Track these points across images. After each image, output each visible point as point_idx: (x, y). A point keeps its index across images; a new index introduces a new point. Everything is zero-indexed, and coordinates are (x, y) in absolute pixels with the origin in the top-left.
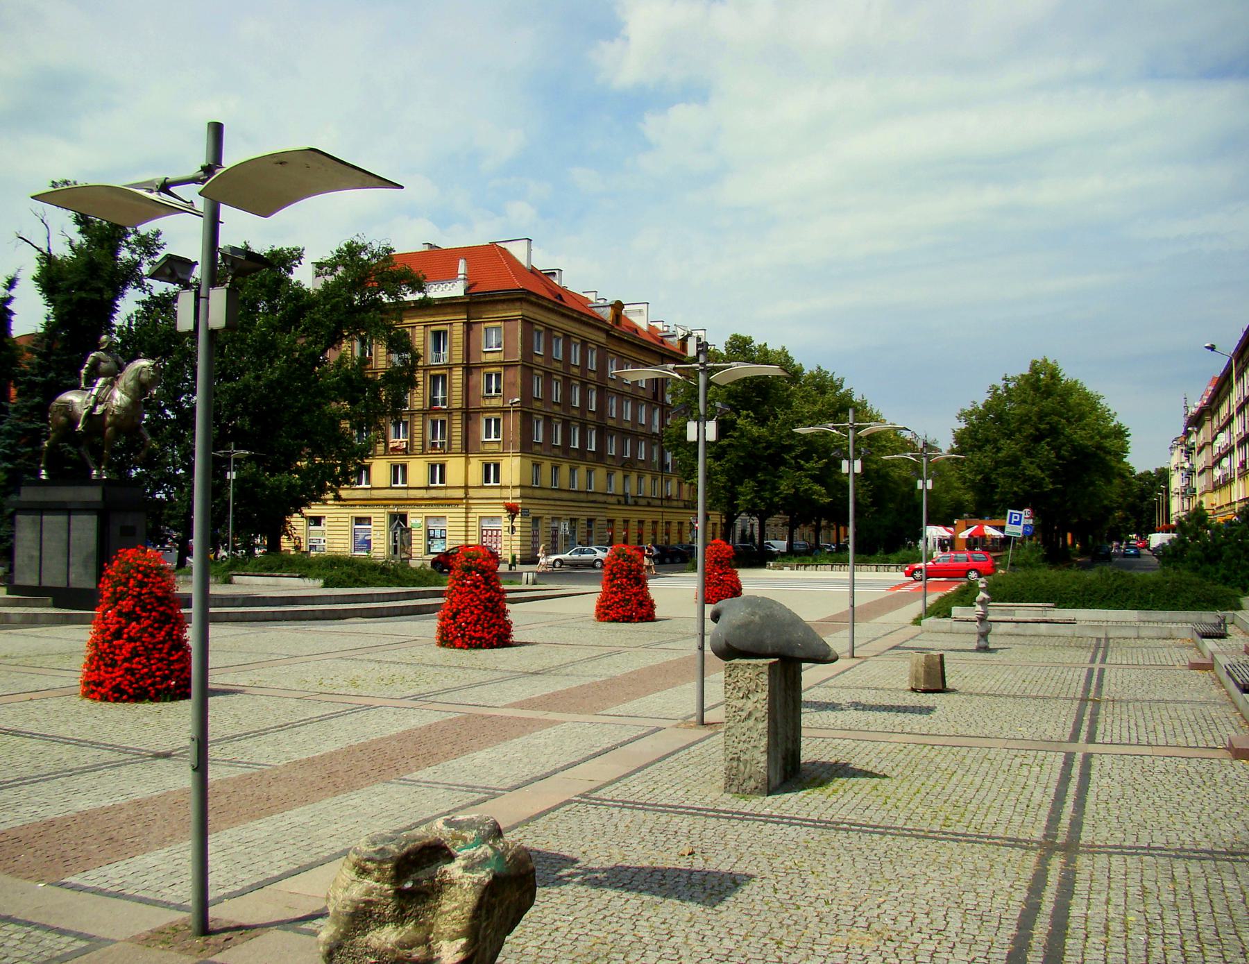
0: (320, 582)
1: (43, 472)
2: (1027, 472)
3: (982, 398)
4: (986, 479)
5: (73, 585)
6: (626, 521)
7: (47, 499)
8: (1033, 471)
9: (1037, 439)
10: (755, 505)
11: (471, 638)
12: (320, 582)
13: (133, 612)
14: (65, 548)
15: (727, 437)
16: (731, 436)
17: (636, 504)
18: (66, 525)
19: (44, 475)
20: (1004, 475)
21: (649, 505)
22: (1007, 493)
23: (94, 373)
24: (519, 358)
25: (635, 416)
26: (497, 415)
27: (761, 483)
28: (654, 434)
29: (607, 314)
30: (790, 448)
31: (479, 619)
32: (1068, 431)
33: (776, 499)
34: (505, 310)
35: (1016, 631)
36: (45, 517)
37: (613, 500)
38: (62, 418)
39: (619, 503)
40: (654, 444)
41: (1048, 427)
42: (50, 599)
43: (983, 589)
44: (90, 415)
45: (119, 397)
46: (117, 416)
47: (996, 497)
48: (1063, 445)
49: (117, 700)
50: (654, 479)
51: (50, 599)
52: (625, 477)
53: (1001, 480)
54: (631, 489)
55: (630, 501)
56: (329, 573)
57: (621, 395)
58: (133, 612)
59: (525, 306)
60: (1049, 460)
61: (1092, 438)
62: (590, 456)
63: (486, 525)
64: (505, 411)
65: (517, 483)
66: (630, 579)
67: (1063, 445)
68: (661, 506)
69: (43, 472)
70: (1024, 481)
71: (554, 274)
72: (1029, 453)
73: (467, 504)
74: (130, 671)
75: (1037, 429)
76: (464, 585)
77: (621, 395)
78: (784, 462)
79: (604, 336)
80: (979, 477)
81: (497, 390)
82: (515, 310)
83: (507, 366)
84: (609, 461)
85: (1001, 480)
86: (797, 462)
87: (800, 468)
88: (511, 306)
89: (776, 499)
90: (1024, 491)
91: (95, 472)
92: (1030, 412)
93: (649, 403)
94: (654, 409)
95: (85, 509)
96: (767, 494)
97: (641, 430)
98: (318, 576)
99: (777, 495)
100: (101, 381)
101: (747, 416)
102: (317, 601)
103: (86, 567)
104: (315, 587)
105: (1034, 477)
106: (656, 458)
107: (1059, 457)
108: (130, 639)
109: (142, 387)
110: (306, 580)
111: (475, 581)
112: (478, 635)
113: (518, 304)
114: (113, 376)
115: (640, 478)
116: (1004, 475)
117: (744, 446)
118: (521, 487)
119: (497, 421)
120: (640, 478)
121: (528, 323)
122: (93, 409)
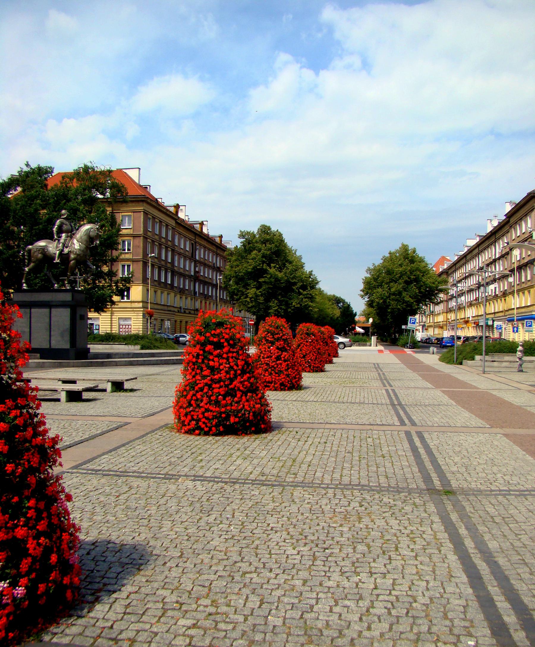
0: (139, 347)
1: (25, 285)
2: (405, 299)
3: (378, 262)
4: (384, 302)
5: (53, 346)
6: (181, 322)
7: (32, 300)
8: (407, 299)
9: (408, 283)
10: (279, 312)
11: (314, 367)
12: (139, 347)
13: (284, 347)
14: (48, 327)
15: (263, 277)
16: (266, 277)
17: (185, 312)
18: (48, 314)
19: (25, 286)
20: (393, 300)
21: (190, 313)
22: (395, 308)
23: (60, 231)
24: (141, 232)
25: (185, 266)
26: (128, 263)
27: (280, 301)
28: (192, 275)
29: (172, 209)
30: (295, 284)
31: (316, 359)
32: (424, 279)
33: (289, 310)
34: (134, 207)
35: (511, 366)
36: (33, 310)
37: (176, 310)
38: (40, 255)
39: (178, 312)
40: (191, 281)
41: (414, 277)
42: (38, 355)
43: (521, 345)
44: (61, 254)
45: (76, 245)
46: (78, 255)
47: (389, 310)
48: (422, 286)
49: (281, 390)
50: (191, 300)
51: (38, 355)
52: (181, 298)
53: (392, 302)
54: (183, 305)
55: (182, 311)
56: (142, 342)
57: (180, 254)
58: (284, 347)
59: (145, 204)
60: (416, 293)
61: (433, 283)
62: (168, 286)
63: (122, 323)
64: (133, 261)
65: (140, 300)
66: (324, 343)
67: (422, 286)
68: (194, 314)
69: (25, 285)
70: (403, 303)
71: (147, 188)
72: (405, 290)
73: (112, 311)
74: (288, 375)
75: (409, 278)
76: (307, 342)
77: (180, 254)
78: (293, 291)
79: (174, 222)
80: (381, 301)
81: (129, 250)
82: (140, 206)
83: (134, 236)
84: (175, 289)
85: (392, 302)
86: (299, 291)
87: (300, 294)
88: (137, 204)
89: (289, 310)
90: (403, 308)
91: (56, 285)
92: (406, 269)
93: (190, 259)
94: (192, 262)
95: (63, 305)
96: (283, 307)
97: (187, 273)
98: (136, 344)
99: (290, 308)
100: (64, 235)
101: (275, 267)
102: (163, 355)
103: (62, 336)
104: (137, 350)
105: (408, 301)
106: (192, 288)
107: (420, 292)
108: (285, 361)
109: (90, 239)
110: (130, 346)
111: (312, 340)
112: (316, 366)
113: (141, 203)
114: (71, 233)
115: (186, 298)
116: (393, 300)
117: (271, 282)
118: (143, 302)
119: (129, 266)
120: (186, 298)
121: (146, 213)
122: (62, 250)
